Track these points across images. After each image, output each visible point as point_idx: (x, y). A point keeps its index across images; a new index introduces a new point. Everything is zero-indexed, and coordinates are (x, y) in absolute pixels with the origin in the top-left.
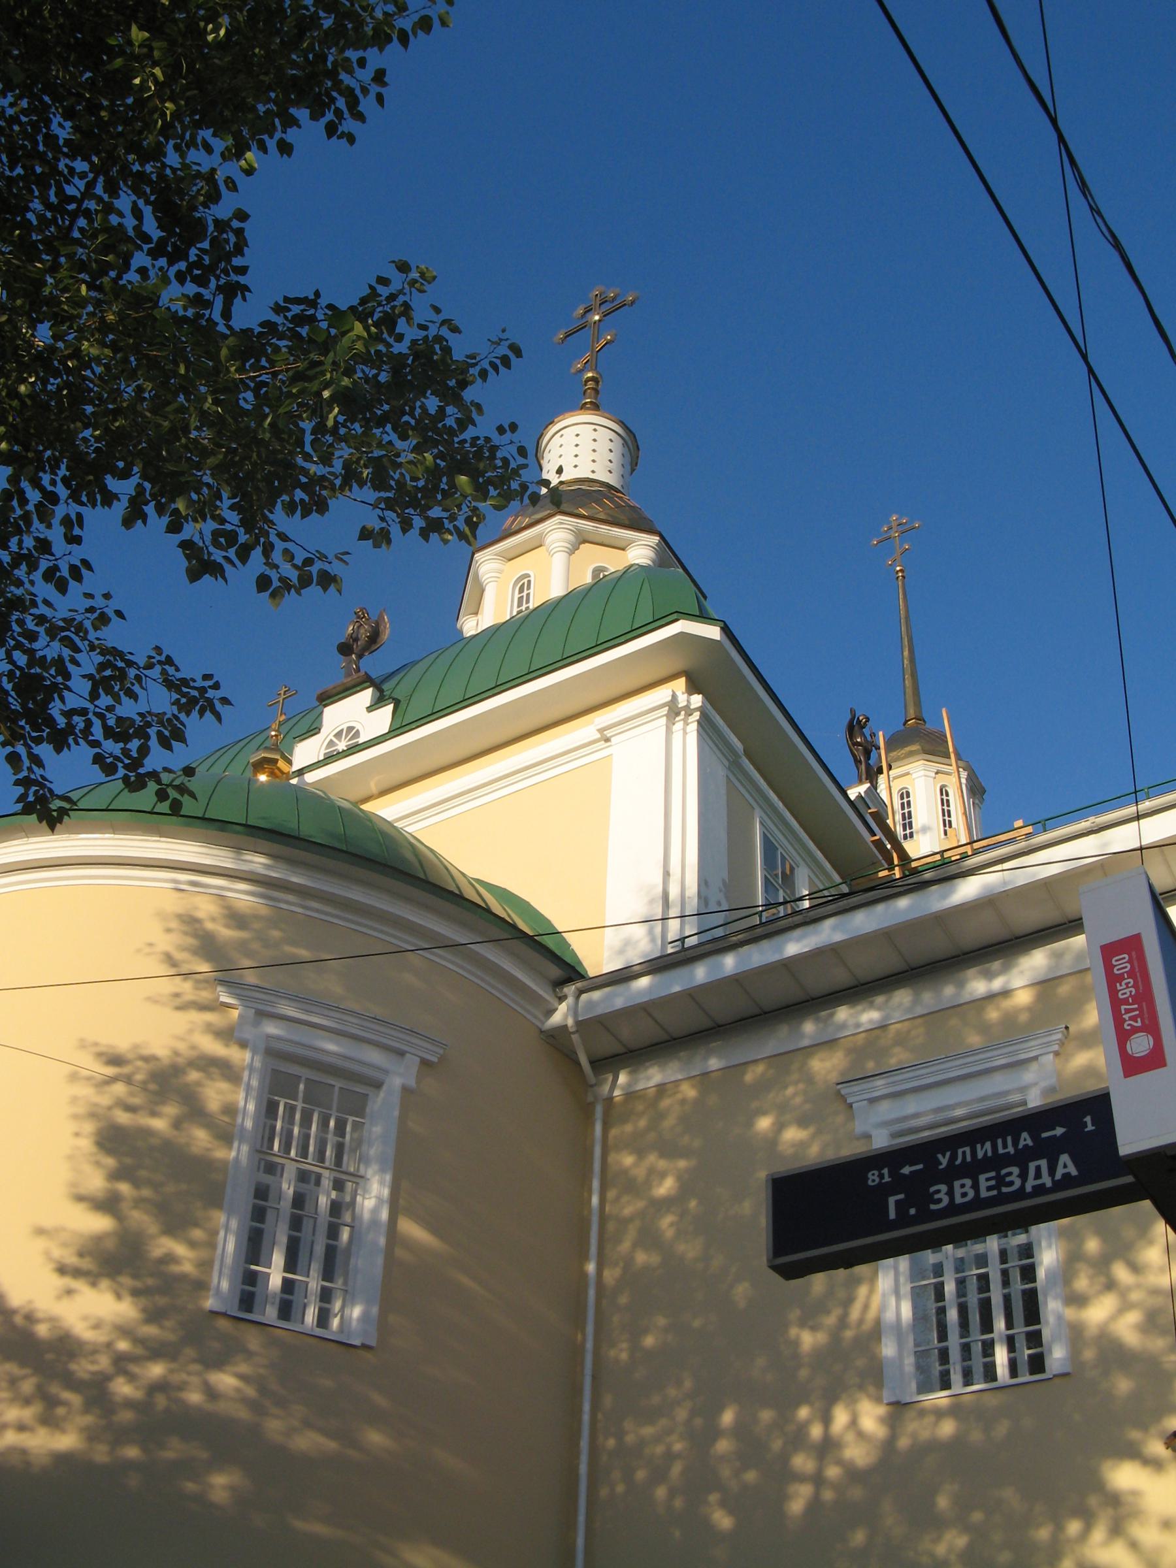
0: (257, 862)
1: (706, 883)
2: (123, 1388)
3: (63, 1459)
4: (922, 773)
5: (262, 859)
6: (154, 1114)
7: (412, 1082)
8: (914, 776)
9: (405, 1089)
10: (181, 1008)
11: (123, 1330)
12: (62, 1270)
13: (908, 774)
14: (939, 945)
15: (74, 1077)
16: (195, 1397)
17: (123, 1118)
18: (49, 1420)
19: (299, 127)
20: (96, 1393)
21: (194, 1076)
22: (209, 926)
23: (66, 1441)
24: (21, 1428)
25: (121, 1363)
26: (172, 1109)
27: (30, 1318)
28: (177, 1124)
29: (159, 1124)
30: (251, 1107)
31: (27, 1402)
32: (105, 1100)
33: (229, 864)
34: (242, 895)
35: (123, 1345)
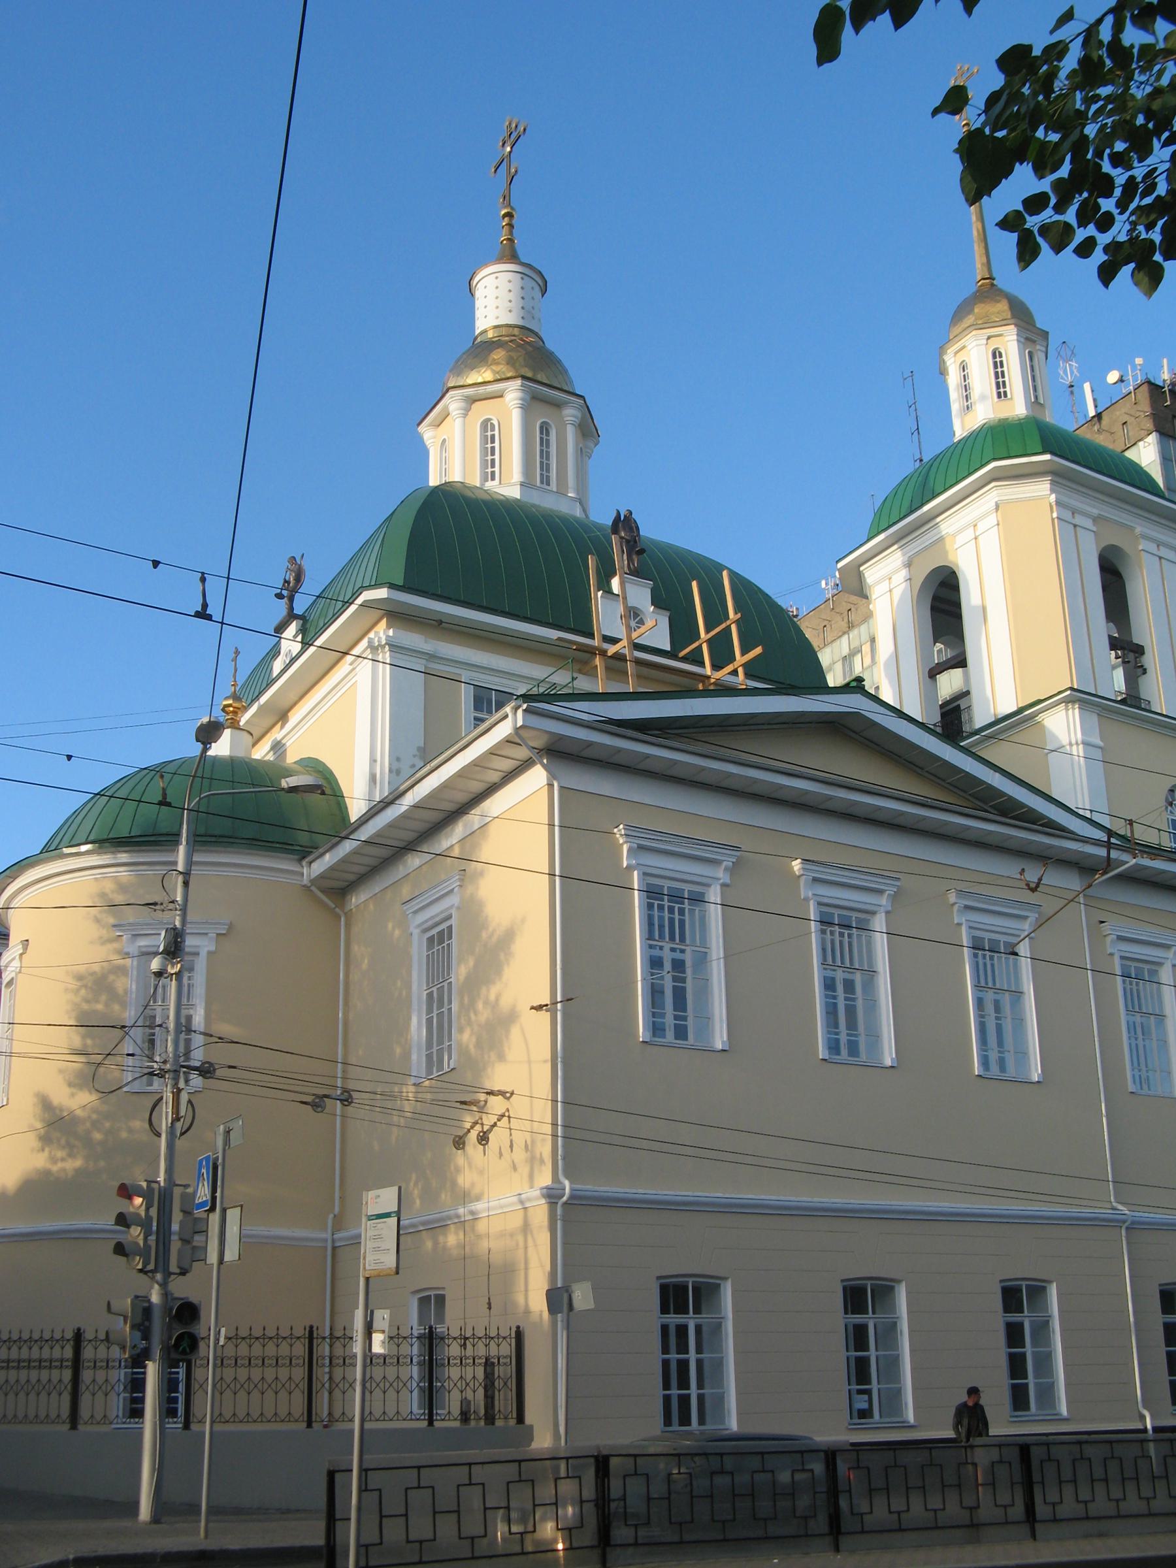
0: (124, 857)
1: (398, 759)
2: (97, 1136)
3: (78, 1171)
4: (974, 343)
5: (124, 855)
6: (97, 1002)
7: (213, 948)
8: (969, 347)
9: (209, 953)
10: (103, 944)
11: (94, 1110)
12: (70, 1085)
13: (964, 347)
14: (435, 817)
15: (66, 990)
16: (124, 1135)
17: (85, 1006)
18: (71, 1155)
19: (896, 29)
20: (88, 1142)
21: (112, 977)
22: (111, 896)
23: (79, 1163)
24: (63, 1160)
25: (95, 1124)
26: (104, 998)
27: (61, 1110)
28: (106, 1005)
29: (100, 1007)
30: (134, 987)
31: (64, 1148)
32: (77, 1000)
33: (113, 862)
34: (123, 873)
35: (94, 1116)
